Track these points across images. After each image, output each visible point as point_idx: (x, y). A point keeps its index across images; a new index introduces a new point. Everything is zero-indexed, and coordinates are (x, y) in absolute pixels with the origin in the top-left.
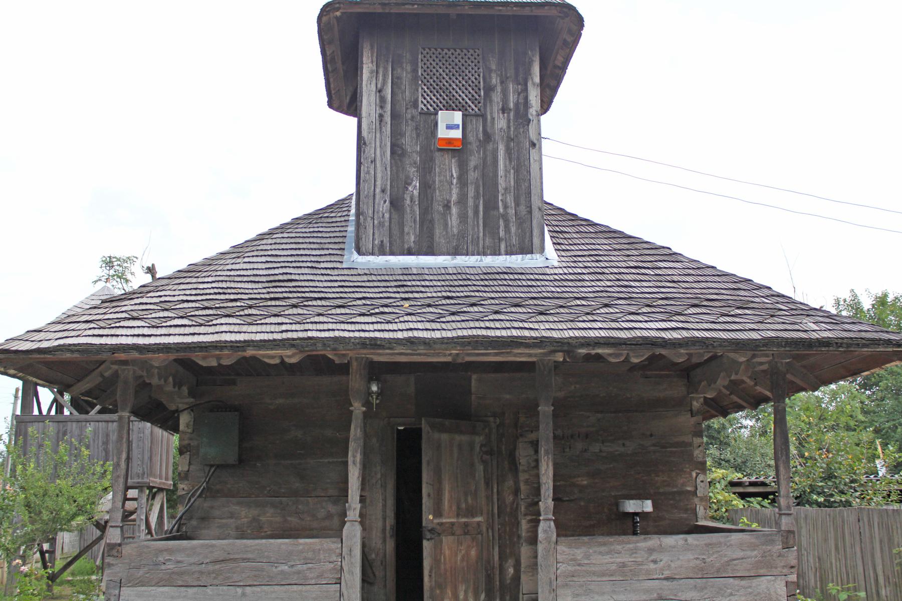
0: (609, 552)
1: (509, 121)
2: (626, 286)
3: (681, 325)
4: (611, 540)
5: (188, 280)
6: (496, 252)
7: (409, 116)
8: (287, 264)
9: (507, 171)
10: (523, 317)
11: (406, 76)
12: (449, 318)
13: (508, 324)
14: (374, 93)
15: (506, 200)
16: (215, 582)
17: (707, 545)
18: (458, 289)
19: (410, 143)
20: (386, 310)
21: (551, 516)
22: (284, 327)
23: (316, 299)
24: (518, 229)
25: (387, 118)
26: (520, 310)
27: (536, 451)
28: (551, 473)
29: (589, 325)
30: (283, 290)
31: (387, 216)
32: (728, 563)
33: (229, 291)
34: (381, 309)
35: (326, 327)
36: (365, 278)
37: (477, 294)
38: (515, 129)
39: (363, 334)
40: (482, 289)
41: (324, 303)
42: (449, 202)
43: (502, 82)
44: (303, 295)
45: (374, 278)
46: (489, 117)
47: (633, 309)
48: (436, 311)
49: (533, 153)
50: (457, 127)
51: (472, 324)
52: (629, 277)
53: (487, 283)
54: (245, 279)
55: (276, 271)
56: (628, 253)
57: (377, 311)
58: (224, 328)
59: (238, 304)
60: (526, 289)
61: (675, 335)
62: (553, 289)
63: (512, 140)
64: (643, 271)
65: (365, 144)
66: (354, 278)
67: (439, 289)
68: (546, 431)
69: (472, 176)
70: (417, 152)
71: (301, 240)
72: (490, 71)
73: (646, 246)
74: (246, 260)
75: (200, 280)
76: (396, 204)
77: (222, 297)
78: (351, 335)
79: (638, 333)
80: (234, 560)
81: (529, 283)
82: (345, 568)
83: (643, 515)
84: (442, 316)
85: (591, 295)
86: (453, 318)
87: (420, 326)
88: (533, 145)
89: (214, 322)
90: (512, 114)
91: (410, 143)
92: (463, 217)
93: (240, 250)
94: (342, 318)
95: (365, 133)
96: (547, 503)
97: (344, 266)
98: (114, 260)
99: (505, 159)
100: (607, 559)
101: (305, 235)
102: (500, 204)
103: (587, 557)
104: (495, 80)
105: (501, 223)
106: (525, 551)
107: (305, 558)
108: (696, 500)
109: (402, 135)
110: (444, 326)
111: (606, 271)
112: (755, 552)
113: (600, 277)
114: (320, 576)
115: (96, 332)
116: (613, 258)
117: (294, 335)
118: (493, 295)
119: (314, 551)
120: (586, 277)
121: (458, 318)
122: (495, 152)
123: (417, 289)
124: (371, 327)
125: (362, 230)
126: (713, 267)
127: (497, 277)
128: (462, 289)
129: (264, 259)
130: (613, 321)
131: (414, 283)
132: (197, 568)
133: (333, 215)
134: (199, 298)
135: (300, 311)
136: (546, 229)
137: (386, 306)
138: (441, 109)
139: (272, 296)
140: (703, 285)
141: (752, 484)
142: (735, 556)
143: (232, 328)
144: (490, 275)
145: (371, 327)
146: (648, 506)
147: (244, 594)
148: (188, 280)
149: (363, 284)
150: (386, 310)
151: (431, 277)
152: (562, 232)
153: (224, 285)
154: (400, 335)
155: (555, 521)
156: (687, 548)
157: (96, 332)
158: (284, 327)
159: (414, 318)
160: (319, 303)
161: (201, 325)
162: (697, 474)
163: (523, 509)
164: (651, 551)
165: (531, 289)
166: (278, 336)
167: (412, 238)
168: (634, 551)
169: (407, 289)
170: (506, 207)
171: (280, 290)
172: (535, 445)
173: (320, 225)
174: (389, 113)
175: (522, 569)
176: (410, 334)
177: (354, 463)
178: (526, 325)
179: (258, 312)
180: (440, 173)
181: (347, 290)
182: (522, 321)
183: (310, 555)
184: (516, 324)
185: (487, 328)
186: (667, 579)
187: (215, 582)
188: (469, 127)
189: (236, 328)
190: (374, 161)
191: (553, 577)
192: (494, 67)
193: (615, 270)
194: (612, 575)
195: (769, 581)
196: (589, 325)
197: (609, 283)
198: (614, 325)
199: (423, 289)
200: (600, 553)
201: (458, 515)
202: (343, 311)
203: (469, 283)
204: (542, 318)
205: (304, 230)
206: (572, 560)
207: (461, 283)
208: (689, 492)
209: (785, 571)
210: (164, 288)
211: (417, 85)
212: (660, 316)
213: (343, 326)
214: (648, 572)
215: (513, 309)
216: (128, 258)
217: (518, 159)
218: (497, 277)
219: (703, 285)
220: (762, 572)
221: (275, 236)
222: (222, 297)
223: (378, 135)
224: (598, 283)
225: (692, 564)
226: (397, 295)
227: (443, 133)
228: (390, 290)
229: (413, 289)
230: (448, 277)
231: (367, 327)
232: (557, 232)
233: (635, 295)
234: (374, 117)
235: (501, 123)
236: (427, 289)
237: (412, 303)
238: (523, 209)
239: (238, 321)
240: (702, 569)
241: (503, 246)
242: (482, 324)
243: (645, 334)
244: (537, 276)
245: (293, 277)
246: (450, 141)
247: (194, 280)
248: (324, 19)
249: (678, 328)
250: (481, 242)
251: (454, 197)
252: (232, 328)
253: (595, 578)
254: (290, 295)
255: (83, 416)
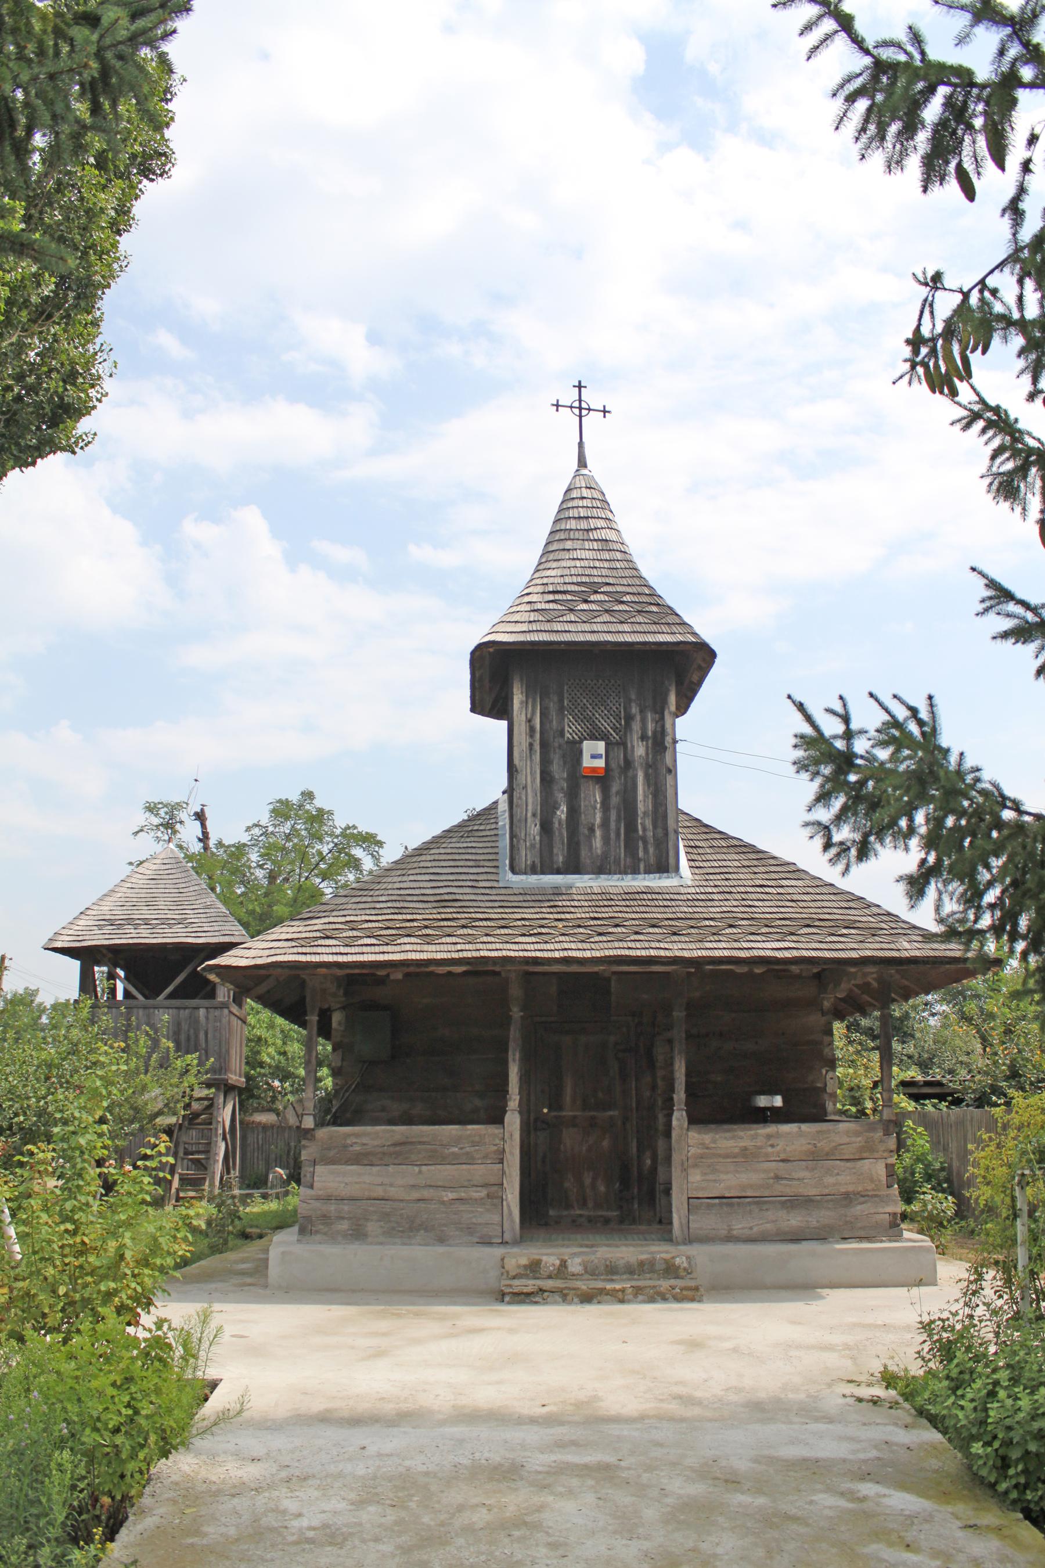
0: (733, 1138)
1: (647, 748)
2: (750, 906)
3: (793, 945)
4: (735, 1127)
5: (364, 899)
6: (635, 871)
7: (556, 745)
8: (450, 883)
9: (645, 796)
10: (659, 937)
11: (553, 707)
12: (597, 939)
13: (647, 945)
14: (523, 723)
15: (644, 823)
16: (396, 1161)
17: (818, 1132)
18: (603, 910)
19: (559, 771)
20: (543, 930)
21: (683, 1107)
22: (459, 947)
23: (481, 920)
24: (655, 850)
25: (537, 747)
26: (656, 930)
27: (672, 1049)
28: (683, 1070)
29: (715, 945)
30: (452, 910)
31: (538, 838)
32: (835, 1148)
33: (404, 911)
34: (539, 930)
35: (494, 946)
36: (521, 898)
37: (620, 915)
38: (653, 756)
39: (526, 954)
40: (624, 909)
41: (489, 923)
42: (593, 825)
43: (641, 711)
44: (470, 915)
45: (528, 898)
46: (629, 745)
47: (753, 929)
48: (585, 931)
49: (669, 778)
50: (599, 756)
51: (616, 944)
52: (753, 896)
53: (628, 903)
54: (415, 898)
55: (442, 891)
56: (756, 870)
57: (535, 931)
58: (408, 947)
59: (415, 924)
60: (662, 910)
61: (787, 954)
62: (686, 910)
63: (650, 766)
64: (767, 890)
65: (517, 771)
66: (512, 898)
67: (587, 909)
68: (678, 1034)
69: (615, 800)
70: (564, 779)
71: (457, 857)
72: (630, 700)
73: (772, 862)
74: (412, 878)
75: (375, 899)
76: (546, 827)
77: (400, 917)
78: (516, 954)
79: (756, 953)
80: (412, 1143)
81: (666, 903)
82: (507, 1150)
83: (773, 1109)
84: (591, 936)
85: (718, 916)
86: (601, 938)
87: (573, 946)
88: (670, 771)
89: (399, 941)
90: (650, 742)
91: (559, 771)
92: (606, 839)
93: (403, 866)
94: (506, 938)
95: (516, 761)
96: (680, 1096)
97: (501, 885)
98: (160, 806)
99: (644, 785)
100: (731, 1143)
101: (460, 851)
102: (640, 827)
103: (714, 1141)
104: (634, 710)
105: (641, 844)
106: (661, 1143)
107: (473, 1142)
108: (826, 1097)
109: (550, 762)
110: (593, 946)
111: (733, 890)
112: (860, 1139)
113: (728, 896)
114: (486, 1157)
115: (300, 950)
116: (742, 876)
117: (469, 955)
118: (633, 916)
119: (480, 1136)
120: (715, 897)
121: (604, 938)
122: (635, 777)
123: (568, 910)
124: (532, 947)
125: (515, 852)
126: (831, 885)
127: (637, 896)
128: (607, 909)
129: (427, 877)
130: (736, 941)
131: (564, 903)
132: (381, 1150)
133: (482, 828)
134: (380, 918)
135: (470, 931)
136: (681, 844)
137: (543, 927)
138: (586, 739)
139: (443, 916)
140: (819, 904)
141: (927, 1084)
142: (842, 1142)
143: (415, 947)
144: (630, 895)
145: (532, 947)
146: (778, 1101)
147: (420, 1172)
148: (364, 899)
149: (520, 904)
150: (543, 930)
151: (579, 897)
152: (696, 847)
153: (398, 905)
154: (557, 955)
155: (687, 1111)
156: (801, 1134)
157: (300, 950)
158: (459, 947)
159: (567, 938)
160: (485, 923)
161: (387, 944)
162: (827, 1072)
163: (660, 1103)
164: (769, 1137)
165: (667, 910)
166: (455, 955)
167: (561, 859)
168: (754, 1137)
169: (559, 910)
170: (644, 829)
171: (448, 910)
172: (670, 1041)
173: (472, 839)
174: (538, 742)
175: (659, 1161)
176: (566, 954)
177: (514, 1060)
178: (662, 945)
179: (434, 933)
180: (585, 798)
181: (507, 910)
182: (659, 941)
183: (477, 1139)
184: (653, 945)
185: (629, 948)
186: (783, 1161)
187: (396, 1161)
188: (611, 755)
189: (419, 948)
190: (525, 787)
191: (685, 1158)
192: (633, 697)
193: (742, 889)
194: (735, 1157)
195: (871, 1163)
196: (715, 945)
197: (735, 903)
198: (736, 945)
199: (572, 910)
200: (725, 1138)
201: (584, 1110)
202: (506, 931)
203: (613, 903)
204: (675, 938)
205: (458, 845)
206: (701, 1144)
207: (606, 903)
208: (819, 1088)
209: (885, 1154)
210: (345, 906)
211: (564, 716)
212: (776, 937)
213: (509, 946)
214: (767, 1155)
215: (651, 930)
216: (177, 804)
217: (656, 784)
218: (637, 896)
219: (819, 904)
220: (865, 1155)
221: (432, 851)
222: (400, 917)
223: (529, 763)
224: (726, 903)
225: (804, 1148)
226: (551, 916)
227: (587, 762)
228: (544, 910)
229: (565, 910)
230: (594, 897)
231: (528, 947)
232: (692, 847)
233: (757, 916)
234: (525, 745)
235: (640, 750)
236: (576, 910)
237: (565, 924)
238: (660, 831)
239: (419, 941)
240: (813, 1153)
241: (642, 866)
242: (625, 945)
243: (762, 953)
244: (670, 897)
245: (458, 897)
246: (594, 769)
247: (369, 899)
248: (477, 653)
249: (790, 948)
250: (622, 862)
251: (598, 821)
252: (415, 947)
253: (721, 1160)
254: (459, 916)
255: (151, 1002)
